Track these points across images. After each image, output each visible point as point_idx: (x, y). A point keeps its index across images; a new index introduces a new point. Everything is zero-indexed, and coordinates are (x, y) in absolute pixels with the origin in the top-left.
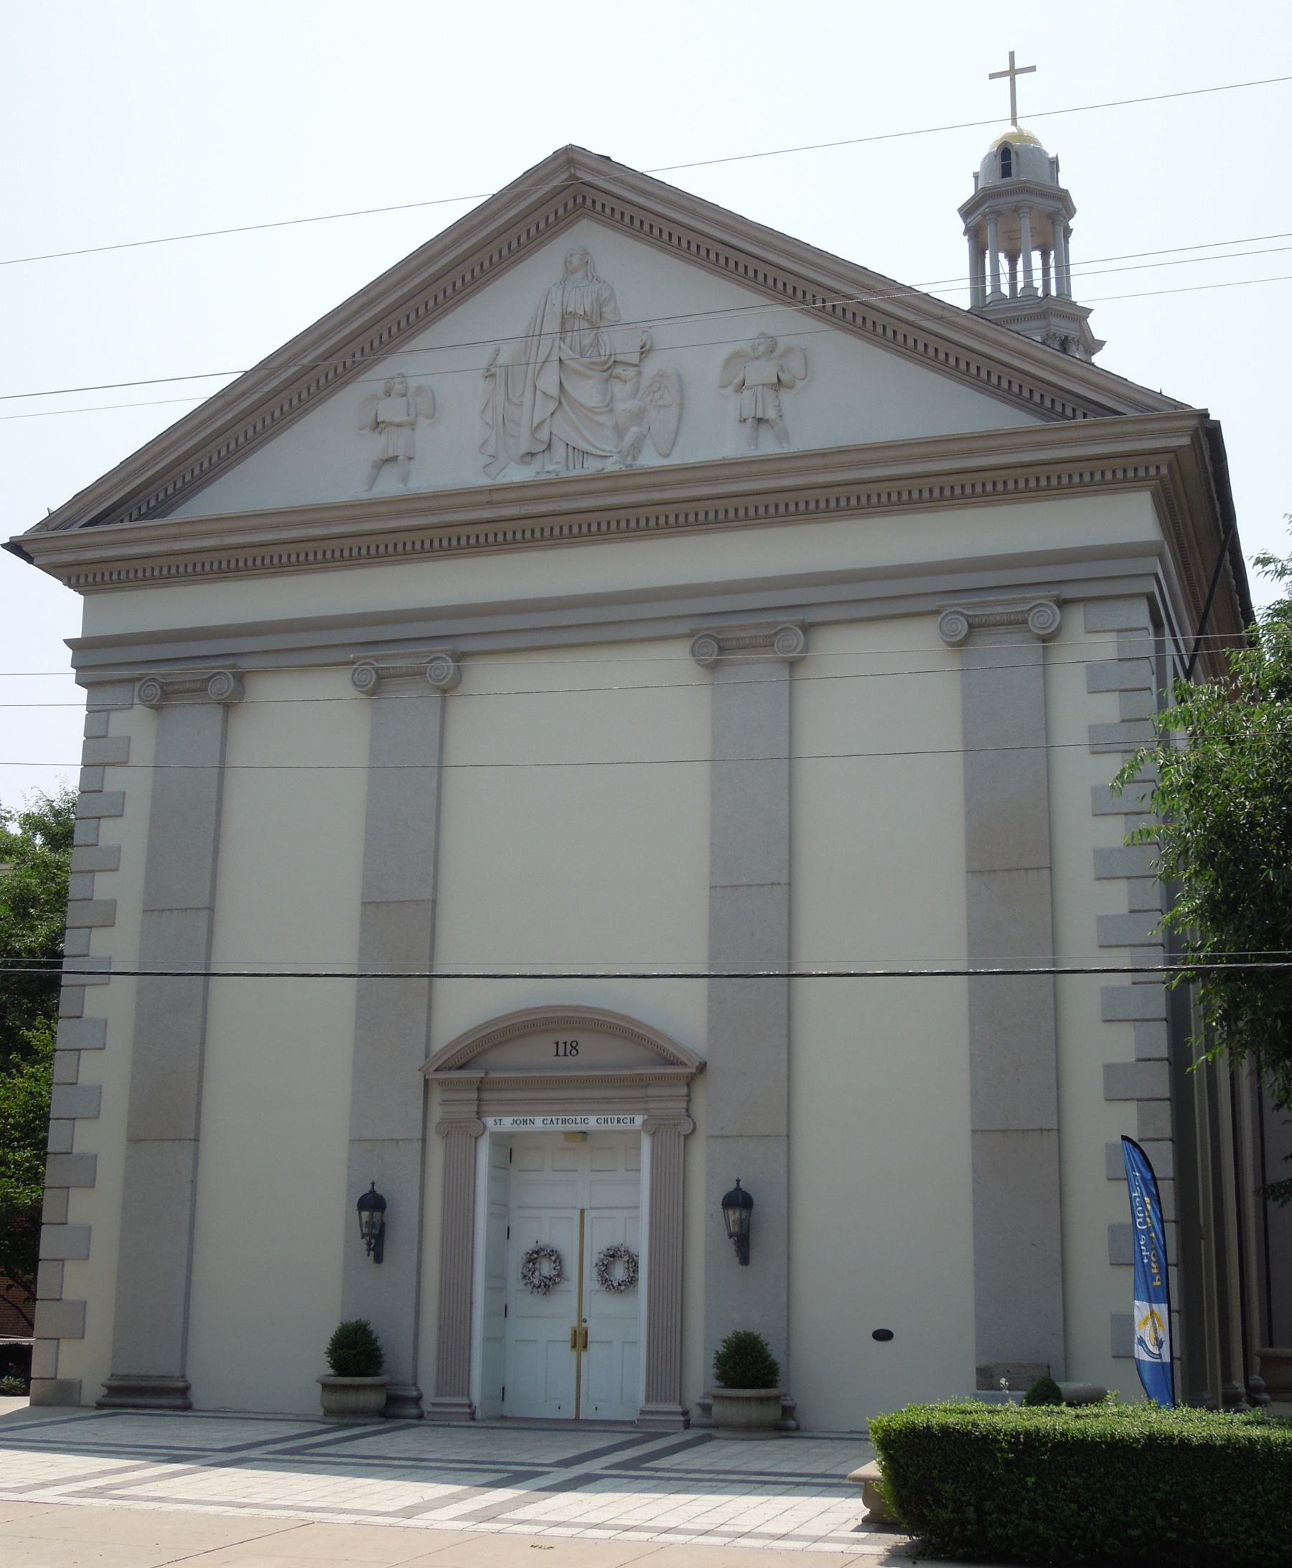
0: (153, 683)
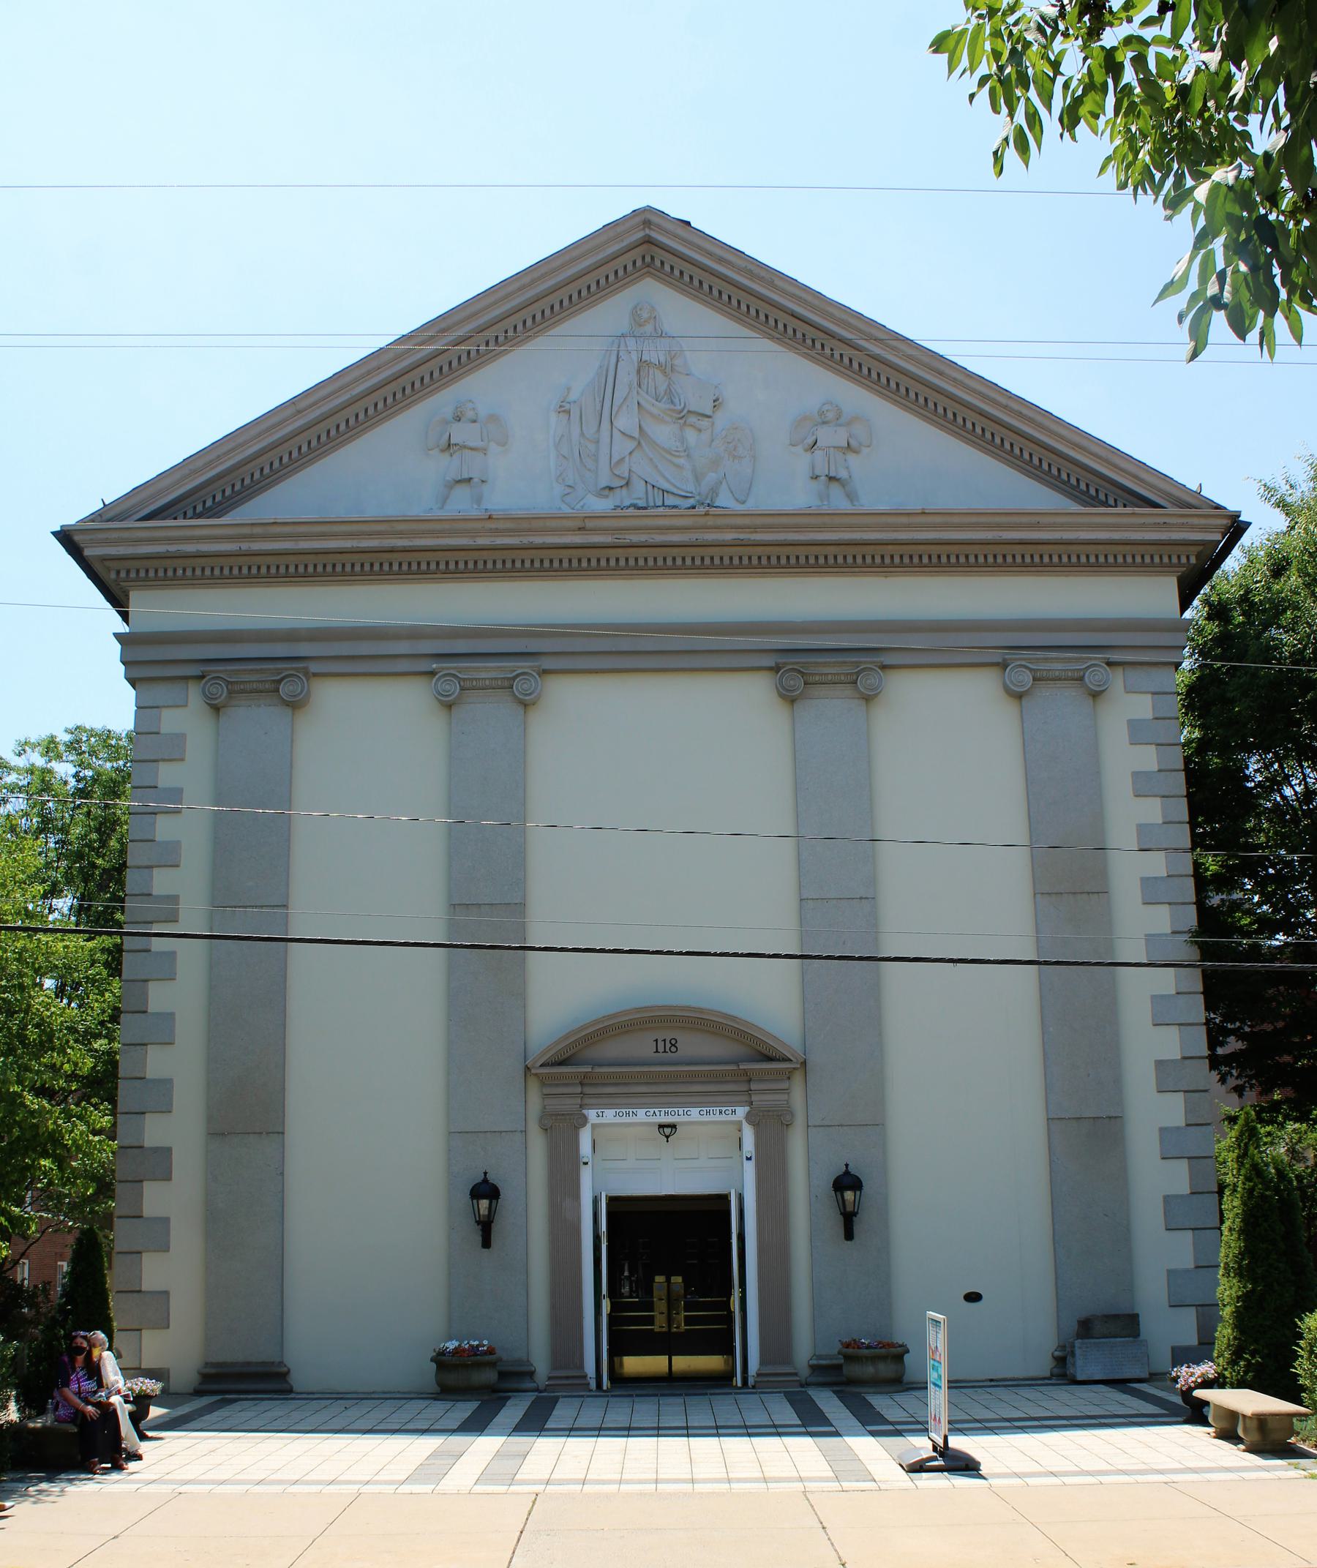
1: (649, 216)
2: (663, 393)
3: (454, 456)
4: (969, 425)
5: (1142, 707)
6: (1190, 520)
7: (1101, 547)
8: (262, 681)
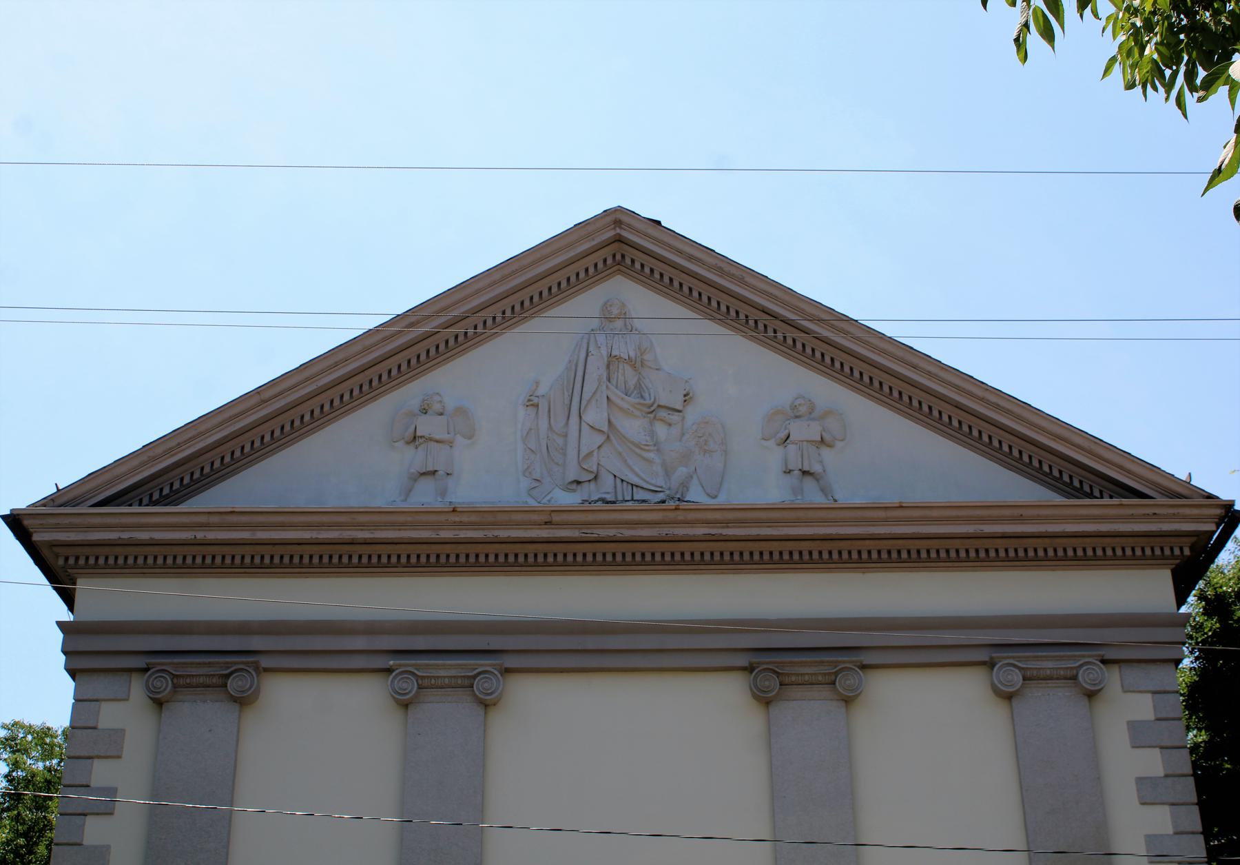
0: (487, 676)
1: (619, 216)
2: (632, 387)
3: (420, 448)
4: (945, 418)
5: (1142, 707)
7: (1088, 540)
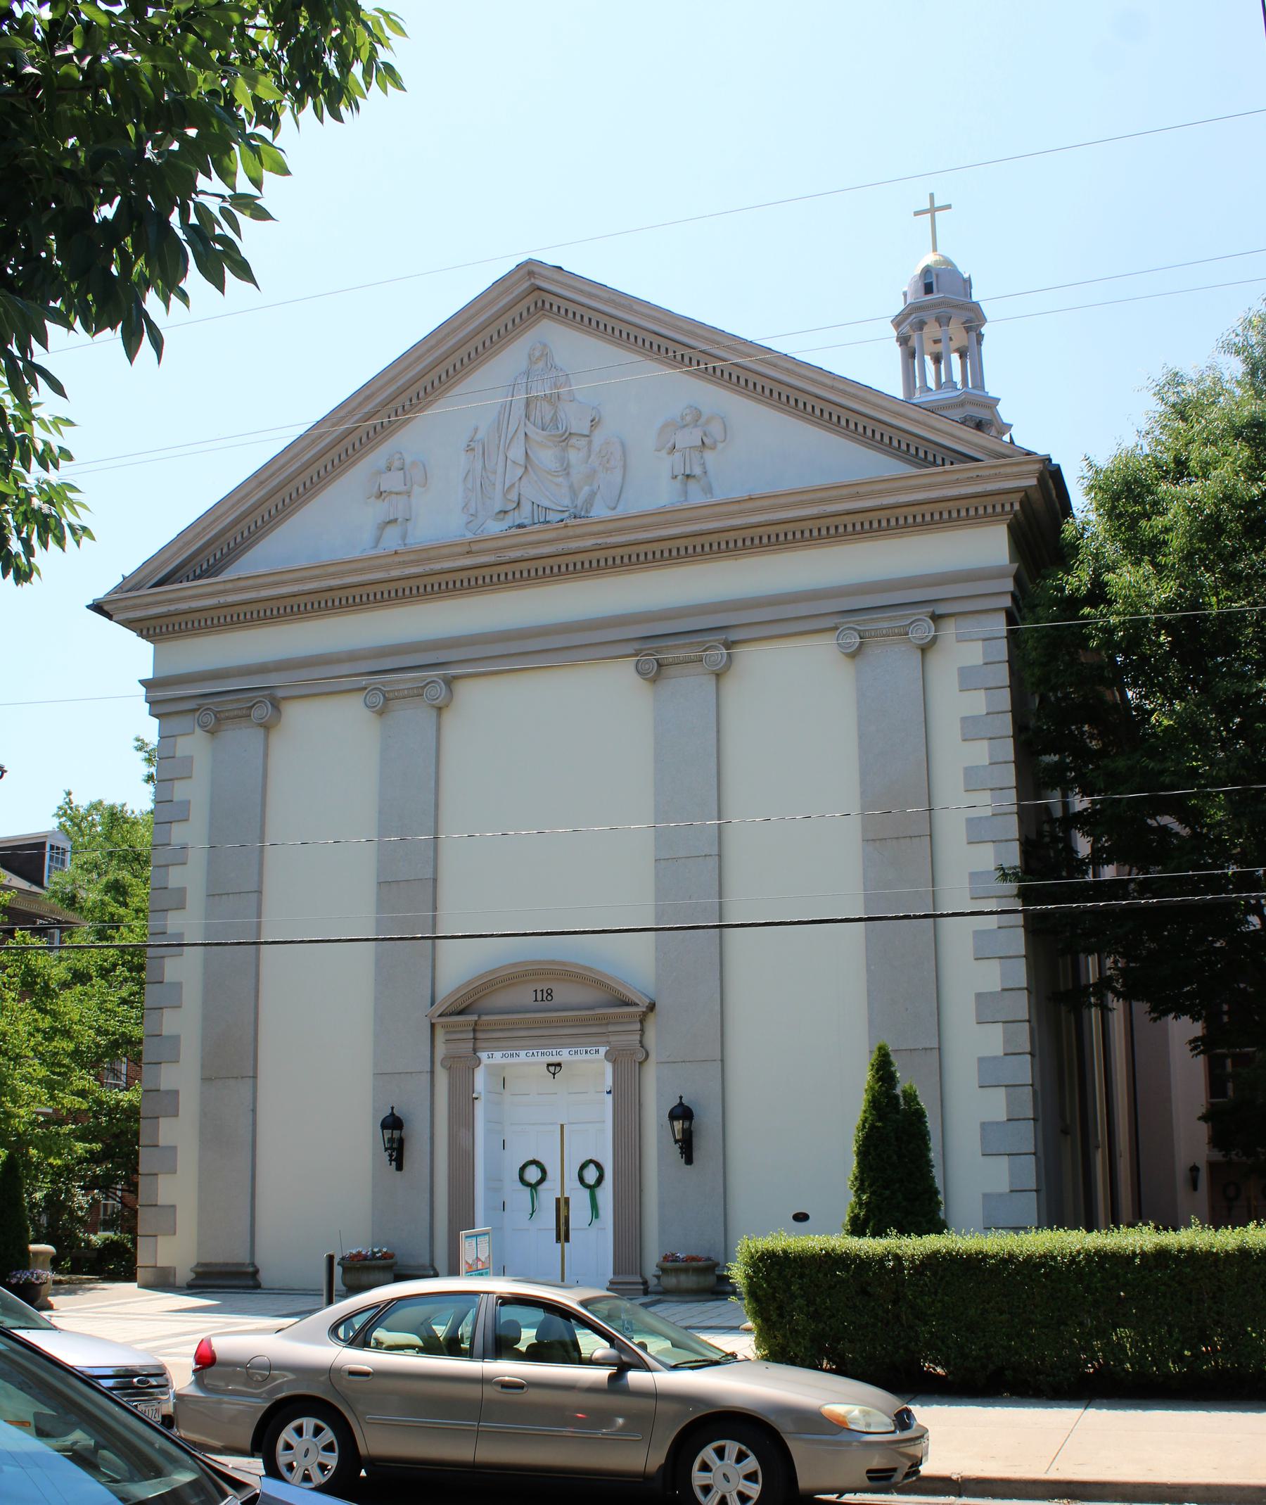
2: (549, 421)
5: (973, 654)
6: (1002, 470)
8: (240, 709)
